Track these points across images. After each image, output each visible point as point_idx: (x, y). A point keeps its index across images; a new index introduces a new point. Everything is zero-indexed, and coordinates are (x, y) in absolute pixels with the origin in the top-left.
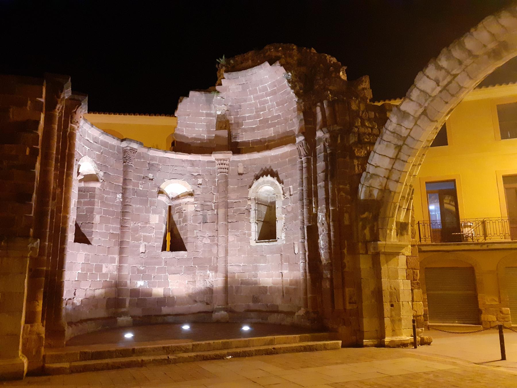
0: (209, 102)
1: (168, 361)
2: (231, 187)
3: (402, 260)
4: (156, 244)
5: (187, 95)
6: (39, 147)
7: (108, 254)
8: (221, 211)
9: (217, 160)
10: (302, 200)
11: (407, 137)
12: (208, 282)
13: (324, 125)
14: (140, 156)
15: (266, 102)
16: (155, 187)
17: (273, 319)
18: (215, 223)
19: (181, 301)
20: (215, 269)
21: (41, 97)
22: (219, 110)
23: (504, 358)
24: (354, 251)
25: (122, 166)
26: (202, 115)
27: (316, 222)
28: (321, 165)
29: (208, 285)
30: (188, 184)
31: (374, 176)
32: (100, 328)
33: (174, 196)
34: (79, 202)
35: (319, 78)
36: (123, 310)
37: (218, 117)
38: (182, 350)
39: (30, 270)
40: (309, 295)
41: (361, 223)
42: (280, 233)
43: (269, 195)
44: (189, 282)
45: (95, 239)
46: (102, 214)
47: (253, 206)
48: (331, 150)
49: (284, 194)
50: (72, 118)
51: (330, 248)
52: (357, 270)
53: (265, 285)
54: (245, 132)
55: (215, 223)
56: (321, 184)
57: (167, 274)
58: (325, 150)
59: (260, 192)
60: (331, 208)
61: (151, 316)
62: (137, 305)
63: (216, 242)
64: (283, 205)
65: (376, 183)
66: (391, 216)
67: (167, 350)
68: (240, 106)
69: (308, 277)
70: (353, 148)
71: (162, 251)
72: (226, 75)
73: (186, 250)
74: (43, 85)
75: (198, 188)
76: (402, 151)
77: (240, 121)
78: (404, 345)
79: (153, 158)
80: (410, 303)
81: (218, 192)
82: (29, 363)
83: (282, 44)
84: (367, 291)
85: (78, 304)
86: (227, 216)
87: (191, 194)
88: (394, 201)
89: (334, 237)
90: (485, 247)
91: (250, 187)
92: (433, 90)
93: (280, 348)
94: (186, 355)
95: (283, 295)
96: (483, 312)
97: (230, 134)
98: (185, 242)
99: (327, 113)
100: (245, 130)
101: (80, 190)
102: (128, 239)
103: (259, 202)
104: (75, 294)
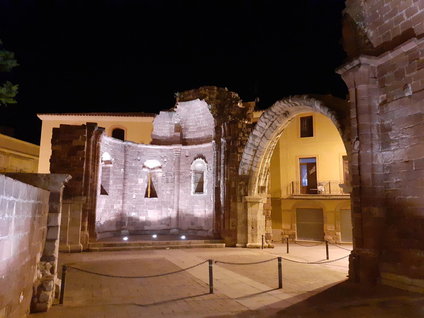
0: (171, 117)
1: (140, 249)
2: (181, 163)
3: (261, 206)
4: (142, 194)
5: (159, 114)
6: (85, 156)
7: (117, 199)
8: (176, 177)
9: (175, 149)
10: (214, 173)
11: (258, 146)
12: (169, 214)
13: (225, 136)
14: (133, 148)
15: (200, 118)
16: (141, 164)
17: (200, 233)
18: (173, 183)
19: (155, 223)
20: (172, 207)
21: (85, 134)
22: (176, 121)
23: (288, 252)
24: (235, 200)
25: (124, 155)
26: (167, 123)
27: (220, 185)
28: (223, 156)
29: (169, 216)
30: (159, 162)
31: (245, 164)
32: (112, 236)
33: (152, 168)
34: (102, 174)
35: (226, 107)
36: (124, 227)
37: (176, 124)
38: (147, 245)
39: (83, 209)
40: (215, 222)
41: (239, 187)
42: (205, 190)
43: (203, 168)
44: (159, 214)
45: (110, 192)
46: (114, 180)
47: (193, 174)
48: (227, 149)
49: (207, 169)
50: (98, 139)
51: (224, 199)
52: (236, 209)
53: (197, 216)
54: (190, 133)
55: (173, 183)
56: (222, 166)
57: (147, 209)
58: (224, 149)
59: (197, 167)
60: (226, 179)
61: (139, 230)
62: (132, 225)
63: (173, 193)
64: (207, 175)
65: (246, 167)
66: (254, 183)
67: (141, 244)
68: (187, 119)
69: (215, 213)
70: (238, 148)
71: (145, 197)
72: (179, 103)
73: (157, 197)
74: (86, 129)
75: (164, 164)
76: (257, 152)
77: (187, 127)
78: (258, 247)
79: (140, 149)
80: (264, 227)
81: (175, 166)
82: (83, 247)
83: (208, 86)
84: (240, 220)
85: (102, 224)
86: (179, 179)
87: (160, 168)
88: (255, 176)
89: (226, 193)
90: (328, 198)
91: (192, 164)
92: (265, 127)
93: (193, 246)
94: (148, 247)
95: (205, 222)
96: (326, 234)
97: (182, 135)
98: (157, 192)
99: (226, 129)
100: (190, 132)
101: (103, 168)
102: (127, 192)
103: (196, 172)
104: (101, 219)
